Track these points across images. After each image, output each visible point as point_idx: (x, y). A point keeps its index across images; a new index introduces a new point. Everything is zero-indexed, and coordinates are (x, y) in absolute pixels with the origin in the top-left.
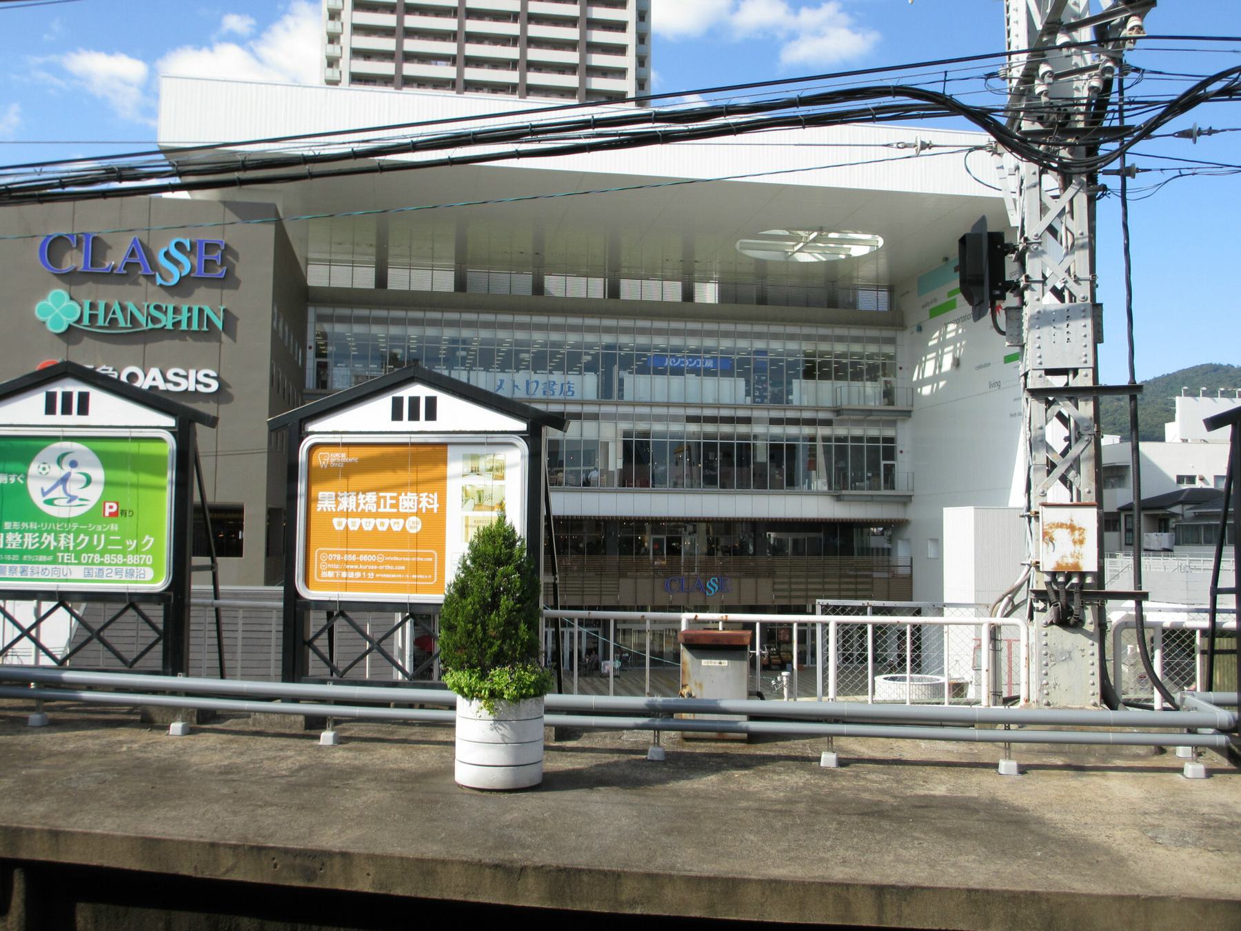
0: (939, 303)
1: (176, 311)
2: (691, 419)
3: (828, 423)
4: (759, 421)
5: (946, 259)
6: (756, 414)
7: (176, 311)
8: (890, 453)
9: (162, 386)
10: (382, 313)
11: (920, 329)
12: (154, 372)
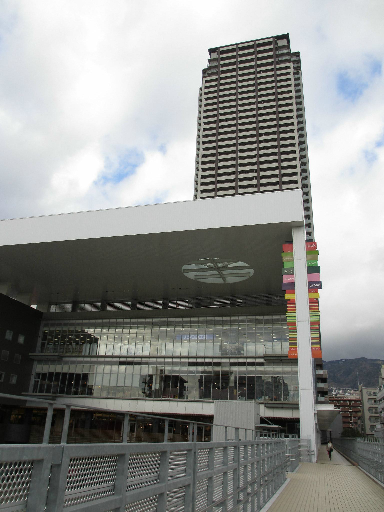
2: (191, 364)
3: (261, 364)
10: (94, 321)
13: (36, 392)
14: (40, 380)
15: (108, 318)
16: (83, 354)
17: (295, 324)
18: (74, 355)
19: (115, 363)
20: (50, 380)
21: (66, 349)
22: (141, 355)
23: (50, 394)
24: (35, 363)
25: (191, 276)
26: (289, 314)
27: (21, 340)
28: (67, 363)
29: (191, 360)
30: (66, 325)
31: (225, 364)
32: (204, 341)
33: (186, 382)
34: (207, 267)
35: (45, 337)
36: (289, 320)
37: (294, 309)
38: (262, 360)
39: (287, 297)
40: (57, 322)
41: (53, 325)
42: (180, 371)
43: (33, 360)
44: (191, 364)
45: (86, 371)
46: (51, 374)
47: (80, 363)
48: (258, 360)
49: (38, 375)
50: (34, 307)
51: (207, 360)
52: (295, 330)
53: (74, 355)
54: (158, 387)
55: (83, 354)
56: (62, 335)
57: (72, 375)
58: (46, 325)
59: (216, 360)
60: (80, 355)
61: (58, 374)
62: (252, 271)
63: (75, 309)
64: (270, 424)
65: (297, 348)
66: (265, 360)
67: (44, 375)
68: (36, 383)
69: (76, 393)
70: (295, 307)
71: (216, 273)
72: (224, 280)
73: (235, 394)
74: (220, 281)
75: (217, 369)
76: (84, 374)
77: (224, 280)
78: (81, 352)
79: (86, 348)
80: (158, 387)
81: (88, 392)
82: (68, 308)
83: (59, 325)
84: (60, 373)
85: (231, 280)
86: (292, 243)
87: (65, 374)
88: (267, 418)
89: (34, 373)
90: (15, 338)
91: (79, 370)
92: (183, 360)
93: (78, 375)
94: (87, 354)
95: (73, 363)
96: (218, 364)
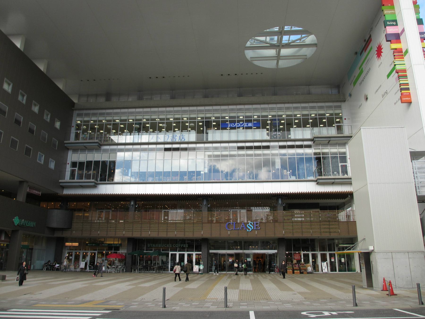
0: (356, 76)
2: (240, 148)
3: (309, 146)
4: (274, 147)
5: (356, 53)
6: (272, 144)
8: (344, 159)
11: (350, 95)
14: (77, 169)
21: (104, 137)
22: (132, 142)
24: (70, 153)
27: (58, 125)
30: (101, 114)
31: (274, 147)
35: (78, 127)
40: (85, 112)
41: (87, 115)
43: (68, 149)
44: (240, 148)
45: (111, 159)
46: (89, 163)
48: (306, 143)
49: (74, 164)
56: (98, 125)
58: (79, 115)
62: (311, 39)
73: (285, 174)
76: (87, 162)
83: (94, 115)
84: (92, 161)
86: (393, 5)
87: (104, 163)
89: (69, 161)
90: (53, 122)
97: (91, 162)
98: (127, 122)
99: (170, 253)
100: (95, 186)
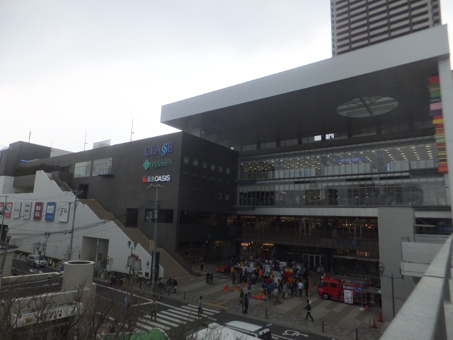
1: (164, 161)
7: (164, 161)
9: (161, 180)
12: (160, 177)
13: (241, 205)
14: (243, 197)
15: (280, 151)
16: (269, 178)
17: (444, 144)
18: (263, 179)
19: (291, 183)
20: (249, 196)
23: (251, 206)
24: (238, 186)
25: (344, 114)
26: (437, 136)
27: (228, 171)
28: (258, 184)
29: (348, 177)
32: (357, 162)
33: (337, 191)
34: (356, 105)
36: (438, 141)
37: (442, 131)
38: (407, 174)
39: (435, 122)
42: (334, 186)
47: (267, 184)
49: (241, 193)
50: (232, 148)
51: (361, 177)
52: (444, 149)
53: (263, 179)
54: (324, 198)
55: (269, 178)
57: (263, 193)
59: (368, 176)
60: (267, 179)
61: (254, 192)
63: (259, 147)
64: (426, 224)
65: (446, 164)
66: (411, 174)
67: (245, 194)
68: (241, 199)
69: (266, 204)
70: (443, 130)
71: (365, 108)
72: (371, 113)
74: (367, 115)
75: (369, 182)
77: (371, 113)
78: (267, 177)
79: (270, 174)
80: (324, 198)
81: (272, 203)
82: (254, 147)
85: (376, 113)
88: (421, 219)
89: (238, 192)
91: (267, 189)
92: (341, 178)
93: (267, 193)
94: (271, 178)
95: (263, 184)
96: (370, 179)
97: (259, 192)
98: (322, 186)
99: (304, 254)
100: (253, 209)
